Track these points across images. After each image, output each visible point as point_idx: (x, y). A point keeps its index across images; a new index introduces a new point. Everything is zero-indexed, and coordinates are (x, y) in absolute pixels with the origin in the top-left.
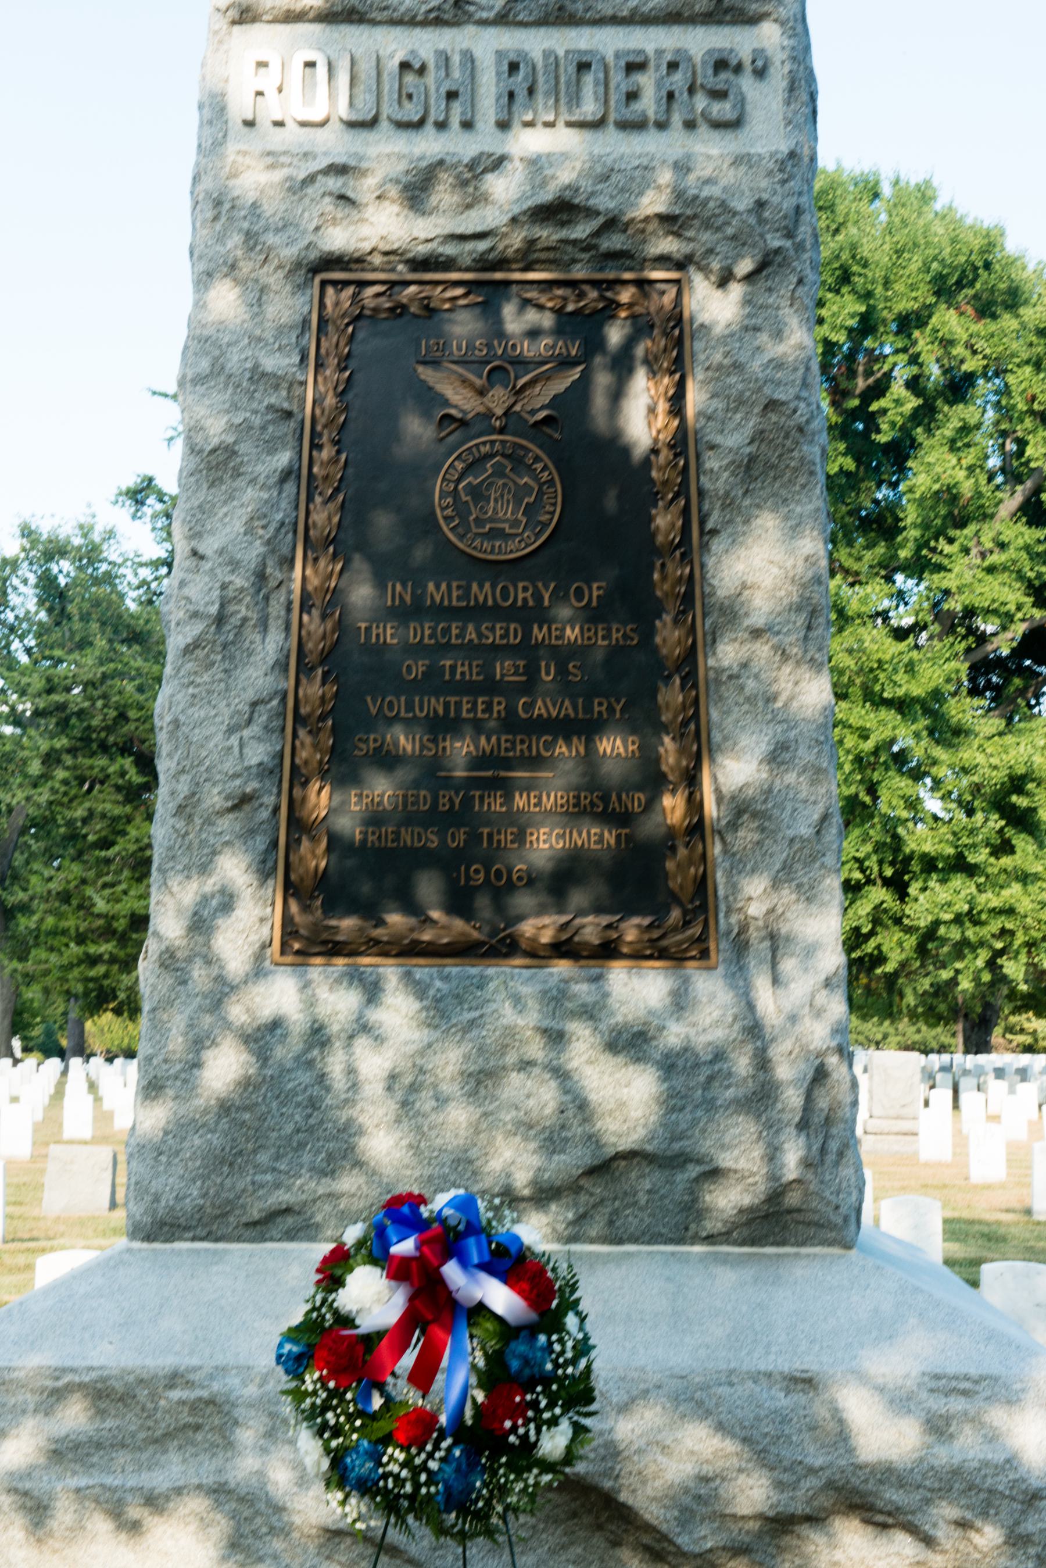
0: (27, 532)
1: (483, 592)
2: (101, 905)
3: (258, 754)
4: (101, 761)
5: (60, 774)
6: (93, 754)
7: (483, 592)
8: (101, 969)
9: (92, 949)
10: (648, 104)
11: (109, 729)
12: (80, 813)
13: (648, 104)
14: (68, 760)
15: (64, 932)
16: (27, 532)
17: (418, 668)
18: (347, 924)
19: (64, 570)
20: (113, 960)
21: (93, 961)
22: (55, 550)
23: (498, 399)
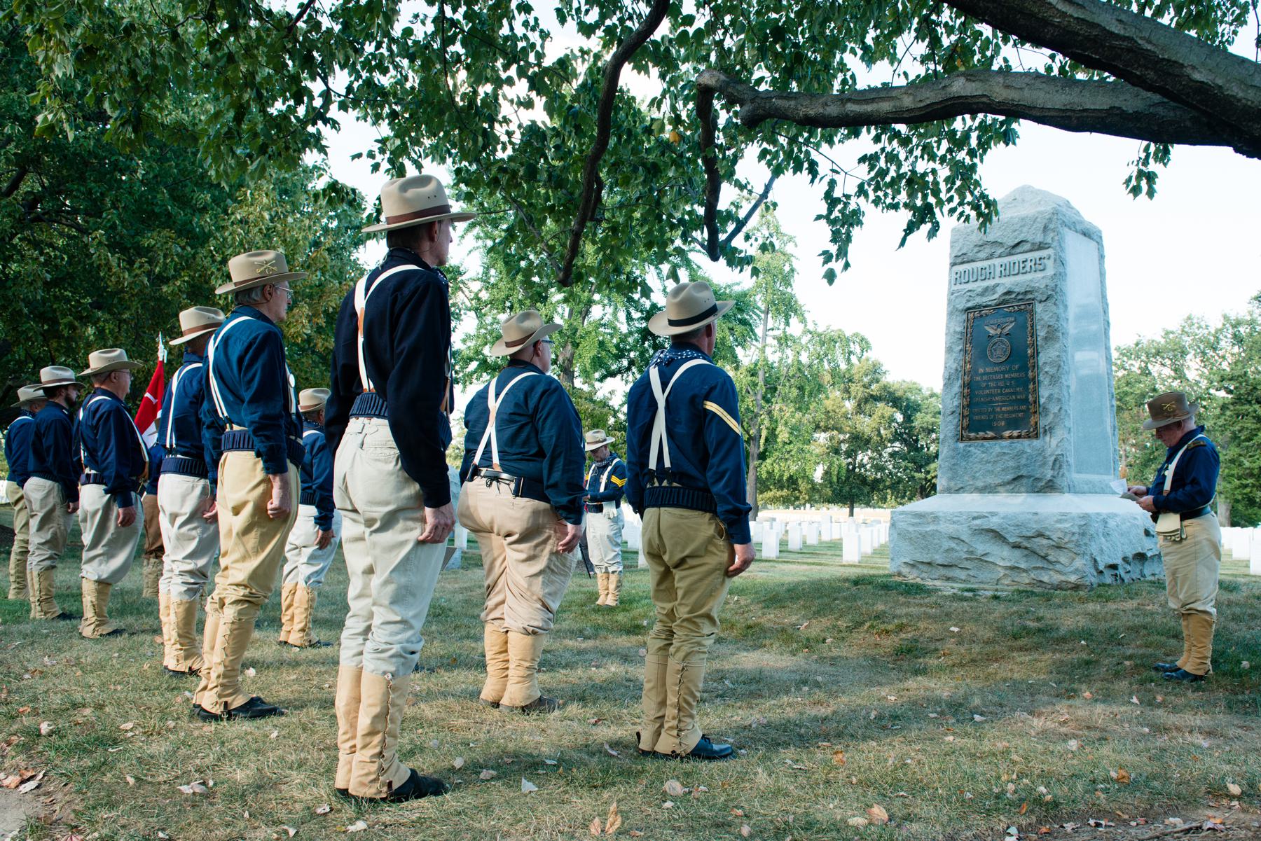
0: (1226, 317)
1: (997, 369)
2: (1247, 464)
3: (956, 403)
4: (1247, 407)
5: (1228, 413)
6: (1243, 404)
7: (997, 369)
8: (1248, 490)
9: (1244, 482)
10: (1028, 268)
11: (1248, 394)
12: (1237, 428)
13: (1028, 268)
14: (1231, 407)
15: (1233, 475)
16: (1226, 317)
17: (984, 385)
18: (972, 435)
19: (1243, 330)
20: (1253, 486)
21: (1246, 486)
22: (1237, 324)
23: (999, 331)
